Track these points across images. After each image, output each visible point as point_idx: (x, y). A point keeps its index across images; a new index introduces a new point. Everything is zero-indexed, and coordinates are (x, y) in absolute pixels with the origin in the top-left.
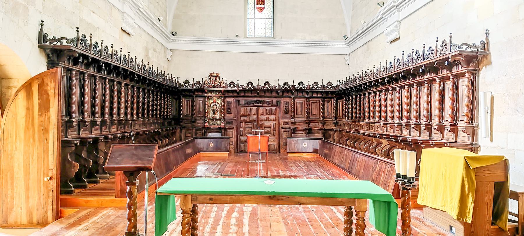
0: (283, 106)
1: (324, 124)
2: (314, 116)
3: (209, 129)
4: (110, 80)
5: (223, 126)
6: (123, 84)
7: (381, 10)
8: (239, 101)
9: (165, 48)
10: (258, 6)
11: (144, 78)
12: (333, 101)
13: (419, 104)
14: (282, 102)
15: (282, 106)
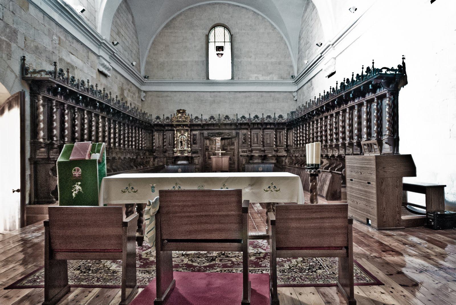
0: (241, 137)
1: (277, 151)
2: (270, 145)
3: (178, 158)
4: (88, 111)
5: (190, 155)
6: (100, 117)
7: (321, 49)
8: (203, 133)
9: (139, 90)
10: (218, 52)
11: (119, 112)
12: (284, 132)
13: (351, 125)
14: (240, 133)
15: (240, 137)
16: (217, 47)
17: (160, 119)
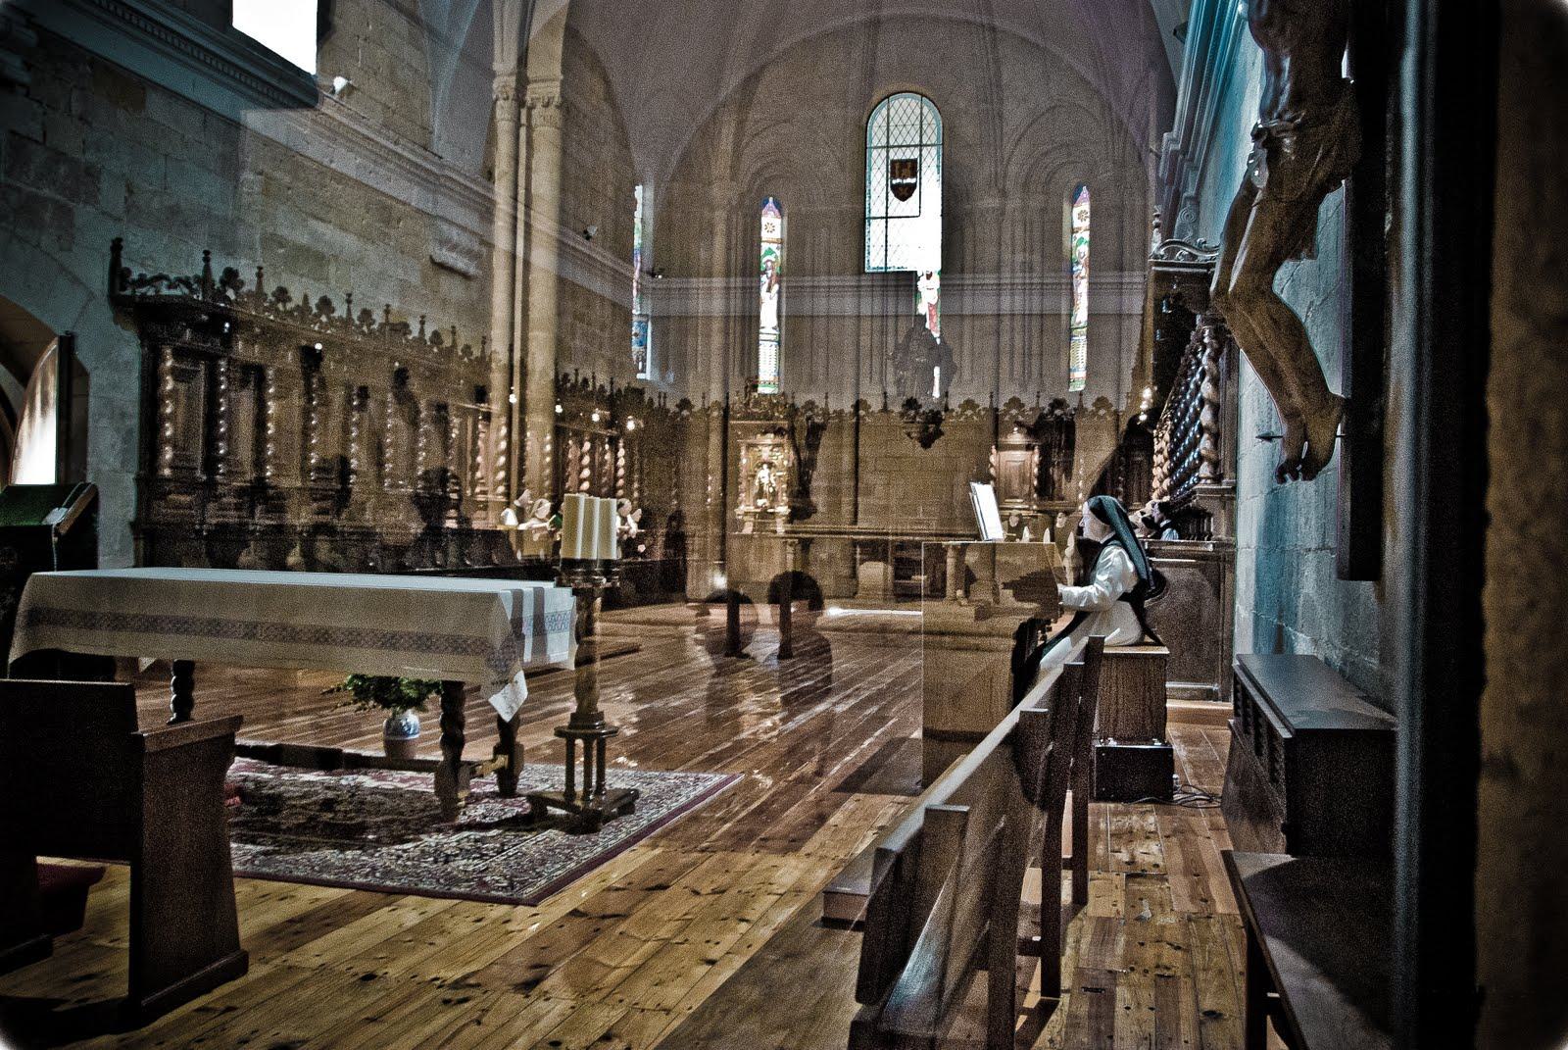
16: (893, 162)
17: (693, 406)
